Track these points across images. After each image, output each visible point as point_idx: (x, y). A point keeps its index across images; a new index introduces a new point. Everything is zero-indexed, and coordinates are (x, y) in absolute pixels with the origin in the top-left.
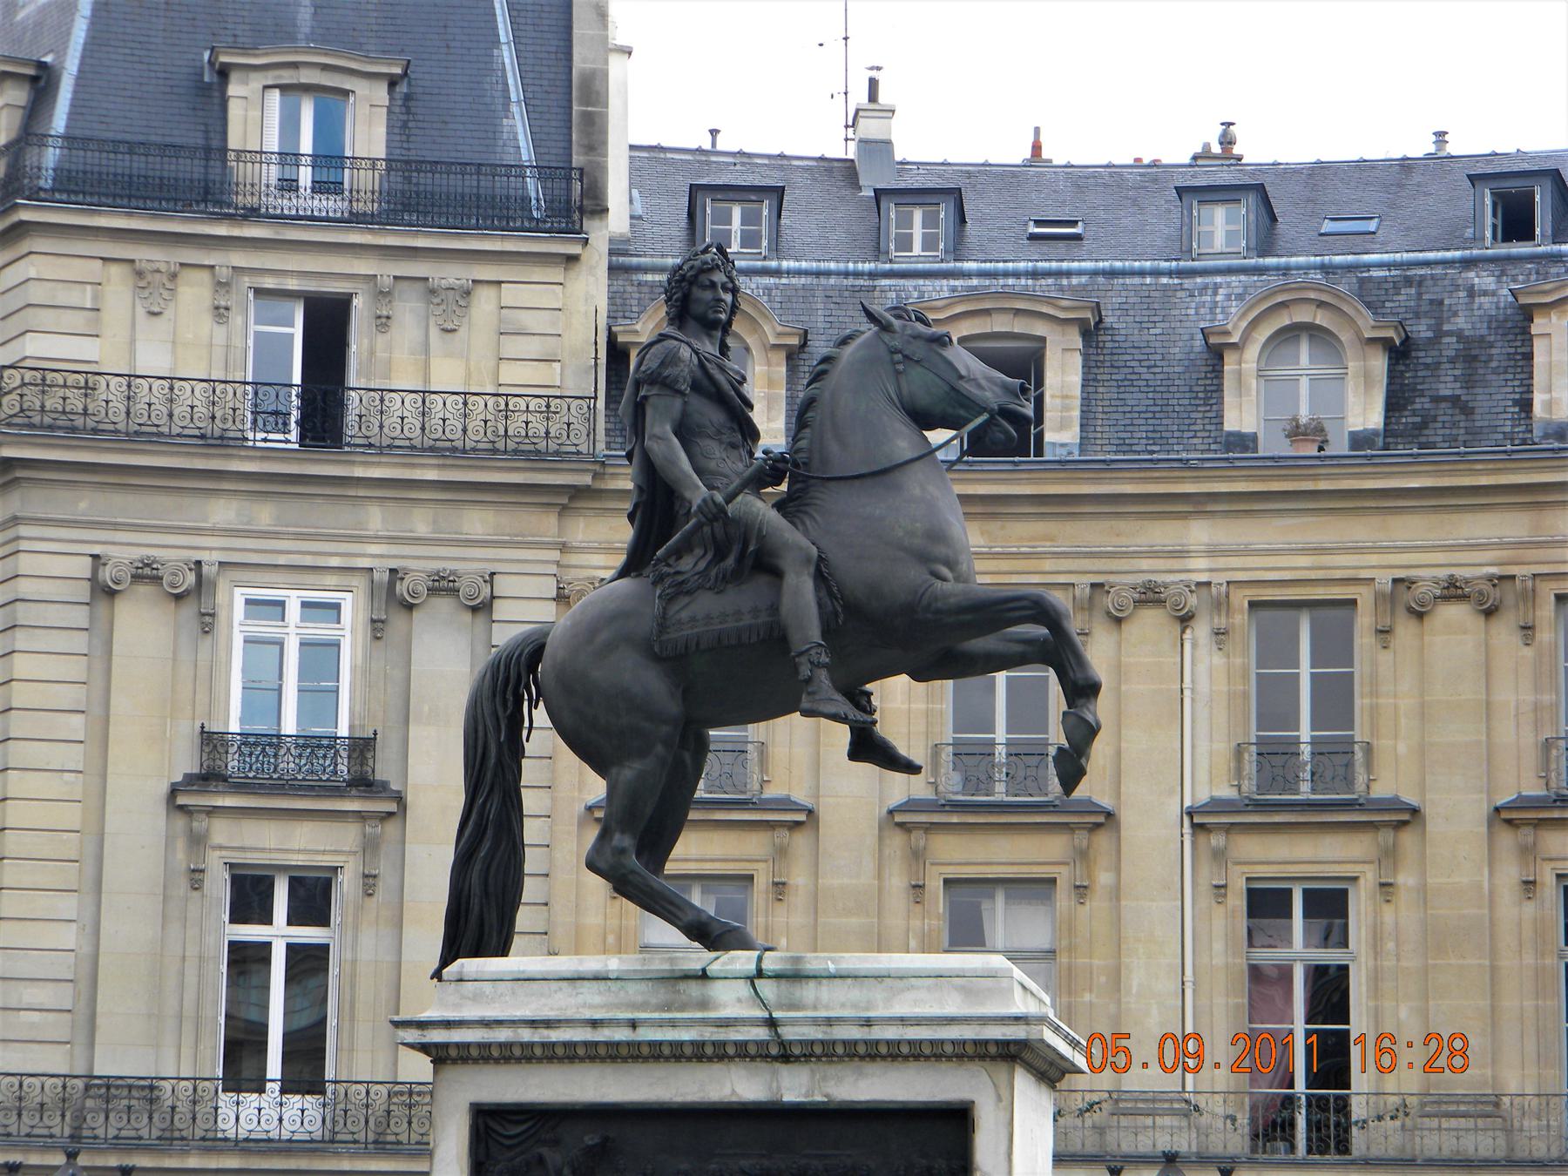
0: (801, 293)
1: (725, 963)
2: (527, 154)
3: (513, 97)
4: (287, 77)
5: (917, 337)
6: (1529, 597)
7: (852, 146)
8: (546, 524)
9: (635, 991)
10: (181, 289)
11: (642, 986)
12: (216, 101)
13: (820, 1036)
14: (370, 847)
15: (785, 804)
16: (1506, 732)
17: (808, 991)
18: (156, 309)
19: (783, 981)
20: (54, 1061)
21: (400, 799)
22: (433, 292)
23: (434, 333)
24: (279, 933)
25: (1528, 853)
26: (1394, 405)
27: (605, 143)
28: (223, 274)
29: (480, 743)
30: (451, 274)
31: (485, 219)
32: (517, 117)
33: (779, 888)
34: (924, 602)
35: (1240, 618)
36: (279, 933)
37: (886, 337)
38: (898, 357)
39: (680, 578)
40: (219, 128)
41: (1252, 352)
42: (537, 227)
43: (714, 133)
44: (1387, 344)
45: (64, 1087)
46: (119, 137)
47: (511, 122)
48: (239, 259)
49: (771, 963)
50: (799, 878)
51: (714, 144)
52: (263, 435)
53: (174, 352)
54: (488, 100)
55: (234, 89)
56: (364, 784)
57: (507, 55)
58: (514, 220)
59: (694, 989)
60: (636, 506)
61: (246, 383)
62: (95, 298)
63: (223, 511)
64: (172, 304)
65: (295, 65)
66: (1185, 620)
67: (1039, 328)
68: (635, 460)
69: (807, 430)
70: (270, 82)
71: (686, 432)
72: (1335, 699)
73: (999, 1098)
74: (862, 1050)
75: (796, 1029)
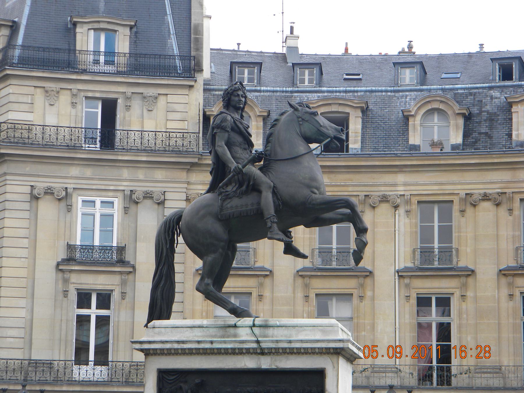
0: (268, 98)
1: (242, 322)
2: (176, 51)
3: (172, 32)
4: (96, 26)
5: (307, 113)
6: (511, 200)
7: (285, 49)
8: (182, 175)
9: (212, 331)
10: (60, 97)
11: (215, 330)
12: (72, 34)
13: (274, 346)
14: (124, 283)
15: (262, 269)
16: (503, 245)
17: (270, 331)
18: (52, 103)
19: (262, 328)
20: (18, 354)
21: (134, 267)
22: (145, 97)
23: (145, 111)
24: (93, 312)
25: (510, 285)
26: (466, 135)
27: (202, 48)
28: (75, 92)
29: (161, 248)
30: (151, 92)
31: (162, 73)
32: (173, 39)
33: (260, 297)
34: (309, 201)
35: (415, 207)
36: (93, 312)
37: (296, 113)
38: (300, 119)
39: (227, 193)
40: (73, 43)
41: (418, 118)
42: (179, 76)
43: (239, 44)
44: (463, 115)
45: (22, 363)
46: (40, 46)
47: (171, 41)
48: (80, 86)
49: (258, 322)
50: (267, 293)
51: (239, 48)
52: (88, 145)
53: (58, 118)
54: (163, 34)
55: (78, 30)
56: (122, 262)
57: (170, 18)
58: (172, 74)
59: (232, 331)
60: (213, 169)
61: (82, 128)
62: (32, 100)
63: (75, 171)
64: (57, 102)
65: (98, 22)
66: (396, 207)
67: (347, 110)
68: (212, 154)
69: (270, 144)
70: (90, 28)
71: (229, 144)
72: (446, 233)
73: (334, 367)
74: (288, 351)
75: (266, 344)
